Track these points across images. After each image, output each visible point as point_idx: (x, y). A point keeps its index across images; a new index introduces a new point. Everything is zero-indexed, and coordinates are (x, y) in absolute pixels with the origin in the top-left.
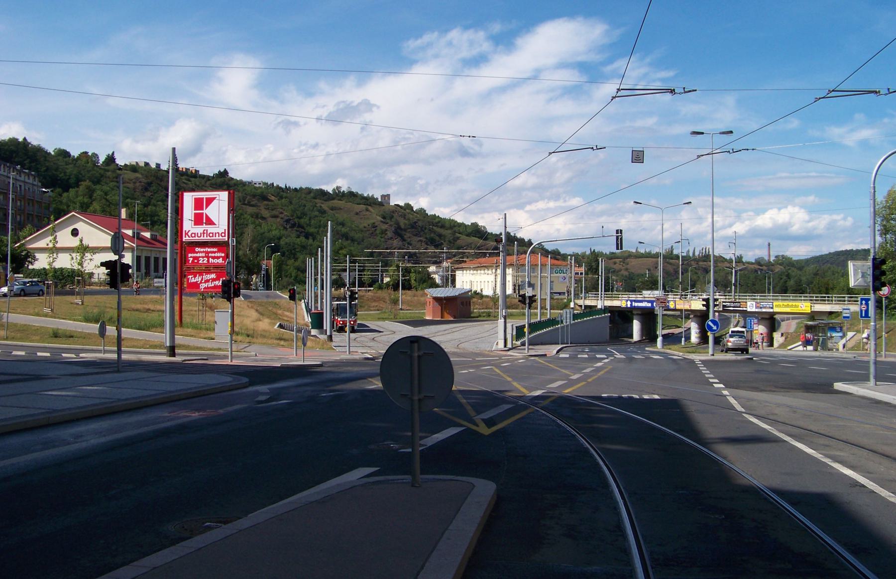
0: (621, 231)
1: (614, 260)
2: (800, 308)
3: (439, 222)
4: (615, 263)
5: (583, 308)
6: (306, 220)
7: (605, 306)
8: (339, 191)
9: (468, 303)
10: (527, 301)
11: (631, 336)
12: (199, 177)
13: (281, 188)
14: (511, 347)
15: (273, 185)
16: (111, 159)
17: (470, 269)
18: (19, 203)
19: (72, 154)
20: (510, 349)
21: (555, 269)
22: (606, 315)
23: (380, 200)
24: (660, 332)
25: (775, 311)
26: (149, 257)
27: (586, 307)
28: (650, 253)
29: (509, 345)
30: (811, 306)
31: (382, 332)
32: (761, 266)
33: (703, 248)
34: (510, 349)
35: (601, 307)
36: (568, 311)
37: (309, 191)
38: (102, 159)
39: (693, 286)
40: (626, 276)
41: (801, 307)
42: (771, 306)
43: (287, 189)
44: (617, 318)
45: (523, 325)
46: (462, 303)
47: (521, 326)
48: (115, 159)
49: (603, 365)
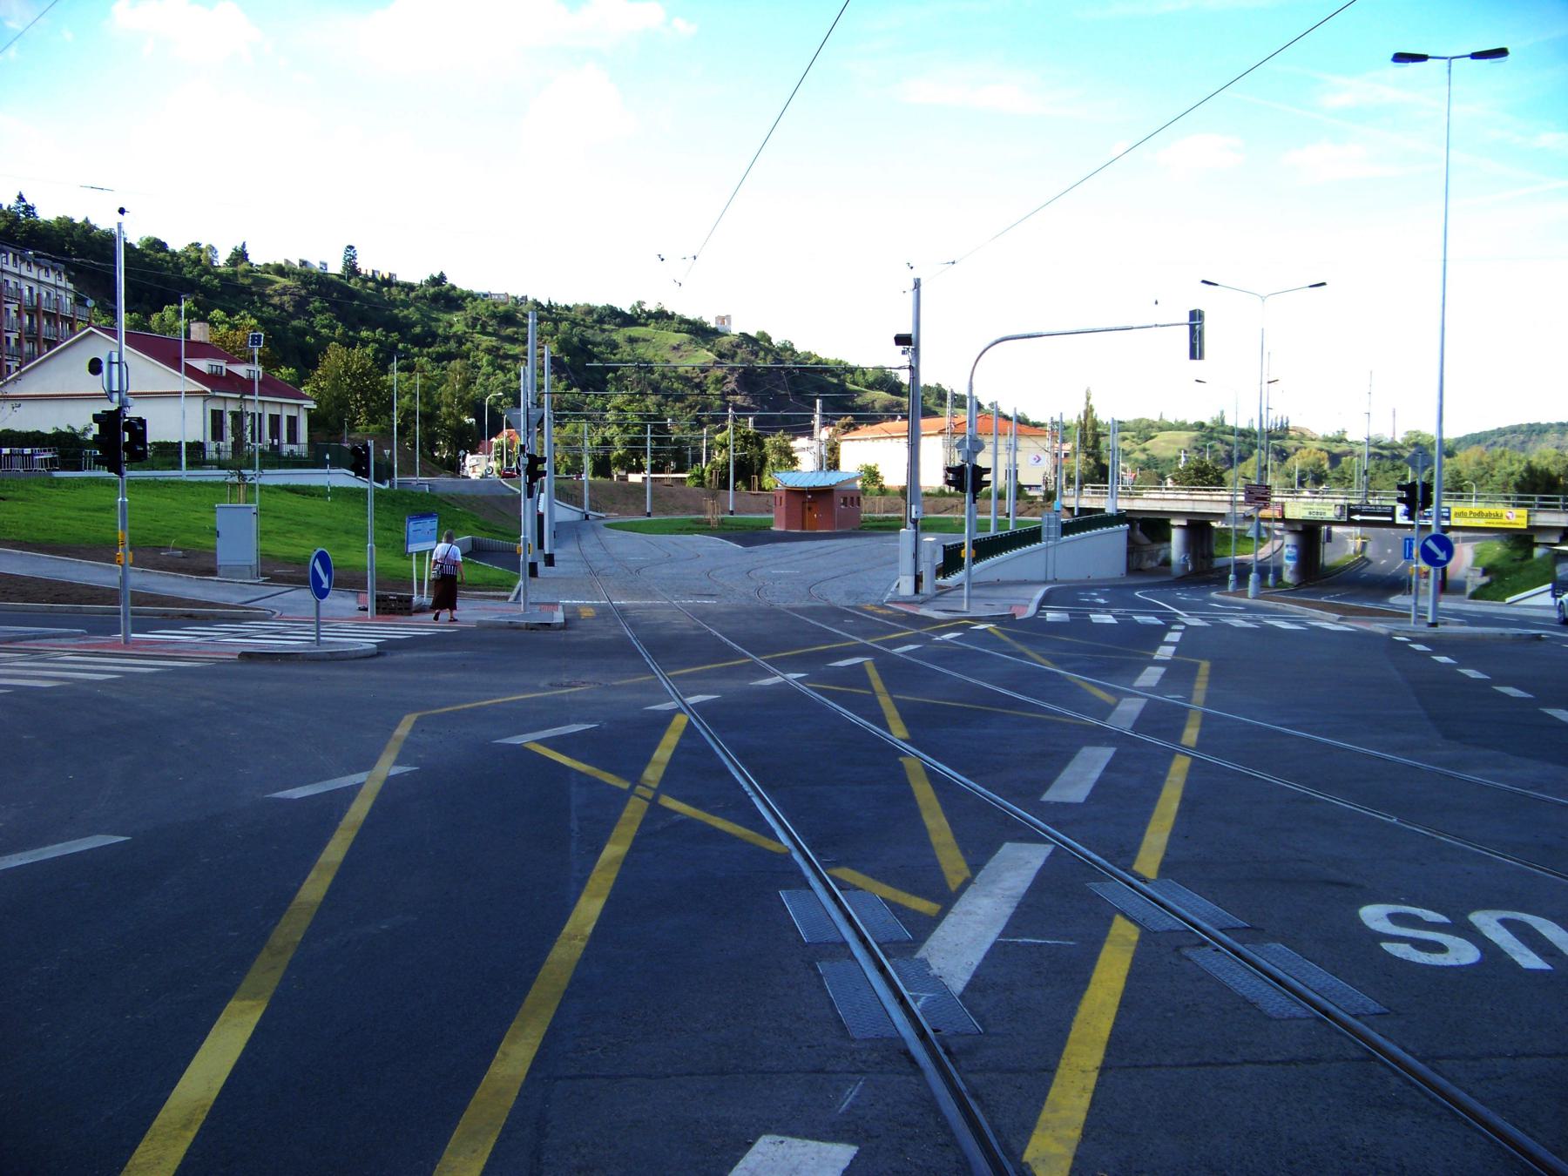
2: (1504, 520)
4: (1124, 439)
8: (642, 310)
9: (855, 499)
15: (527, 300)
16: (240, 255)
18: (27, 320)
19: (171, 247)
25: (1453, 524)
26: (278, 416)
27: (1082, 511)
28: (1184, 424)
29: (926, 588)
30: (1529, 516)
38: (222, 259)
40: (1143, 462)
41: (1508, 518)
42: (1447, 515)
44: (1138, 533)
45: (960, 544)
47: (956, 545)
48: (247, 255)
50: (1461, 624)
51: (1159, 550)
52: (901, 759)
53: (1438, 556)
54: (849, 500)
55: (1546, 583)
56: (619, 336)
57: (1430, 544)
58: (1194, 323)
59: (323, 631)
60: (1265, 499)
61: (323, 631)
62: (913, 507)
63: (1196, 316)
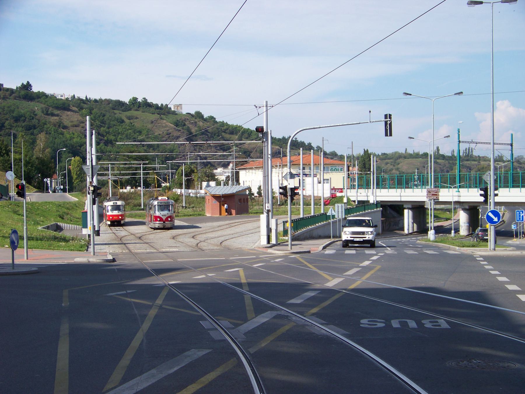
0: (390, 115)
1: (387, 160)
3: (227, 129)
4: (387, 164)
5: (356, 203)
6: (105, 129)
7: (377, 201)
9: (246, 200)
10: (289, 193)
11: (402, 229)
12: (3, 90)
13: (82, 100)
14: (275, 243)
17: (251, 168)
20: (274, 245)
21: (331, 168)
22: (378, 209)
23: (173, 109)
24: (431, 223)
29: (273, 241)
31: (201, 228)
32: (521, 164)
33: (466, 149)
34: (274, 245)
35: (373, 202)
36: (340, 205)
37: (109, 102)
39: (483, 168)
43: (87, 101)
46: (240, 200)
49: (370, 264)
50: (513, 250)
51: (399, 220)
52: (244, 295)
53: (493, 219)
54: (242, 200)
55: (293, 225)
56: (124, 115)
57: (490, 214)
58: (387, 120)
59: (11, 267)
60: (436, 195)
61: (11, 267)
62: (266, 204)
63: (388, 117)
